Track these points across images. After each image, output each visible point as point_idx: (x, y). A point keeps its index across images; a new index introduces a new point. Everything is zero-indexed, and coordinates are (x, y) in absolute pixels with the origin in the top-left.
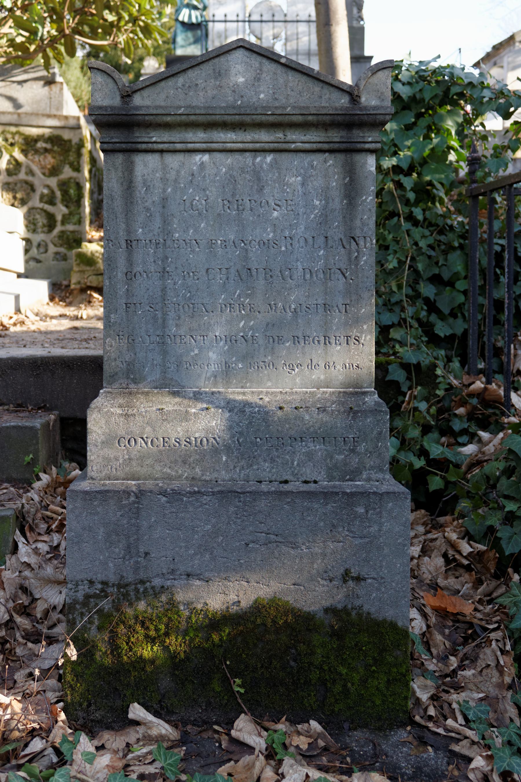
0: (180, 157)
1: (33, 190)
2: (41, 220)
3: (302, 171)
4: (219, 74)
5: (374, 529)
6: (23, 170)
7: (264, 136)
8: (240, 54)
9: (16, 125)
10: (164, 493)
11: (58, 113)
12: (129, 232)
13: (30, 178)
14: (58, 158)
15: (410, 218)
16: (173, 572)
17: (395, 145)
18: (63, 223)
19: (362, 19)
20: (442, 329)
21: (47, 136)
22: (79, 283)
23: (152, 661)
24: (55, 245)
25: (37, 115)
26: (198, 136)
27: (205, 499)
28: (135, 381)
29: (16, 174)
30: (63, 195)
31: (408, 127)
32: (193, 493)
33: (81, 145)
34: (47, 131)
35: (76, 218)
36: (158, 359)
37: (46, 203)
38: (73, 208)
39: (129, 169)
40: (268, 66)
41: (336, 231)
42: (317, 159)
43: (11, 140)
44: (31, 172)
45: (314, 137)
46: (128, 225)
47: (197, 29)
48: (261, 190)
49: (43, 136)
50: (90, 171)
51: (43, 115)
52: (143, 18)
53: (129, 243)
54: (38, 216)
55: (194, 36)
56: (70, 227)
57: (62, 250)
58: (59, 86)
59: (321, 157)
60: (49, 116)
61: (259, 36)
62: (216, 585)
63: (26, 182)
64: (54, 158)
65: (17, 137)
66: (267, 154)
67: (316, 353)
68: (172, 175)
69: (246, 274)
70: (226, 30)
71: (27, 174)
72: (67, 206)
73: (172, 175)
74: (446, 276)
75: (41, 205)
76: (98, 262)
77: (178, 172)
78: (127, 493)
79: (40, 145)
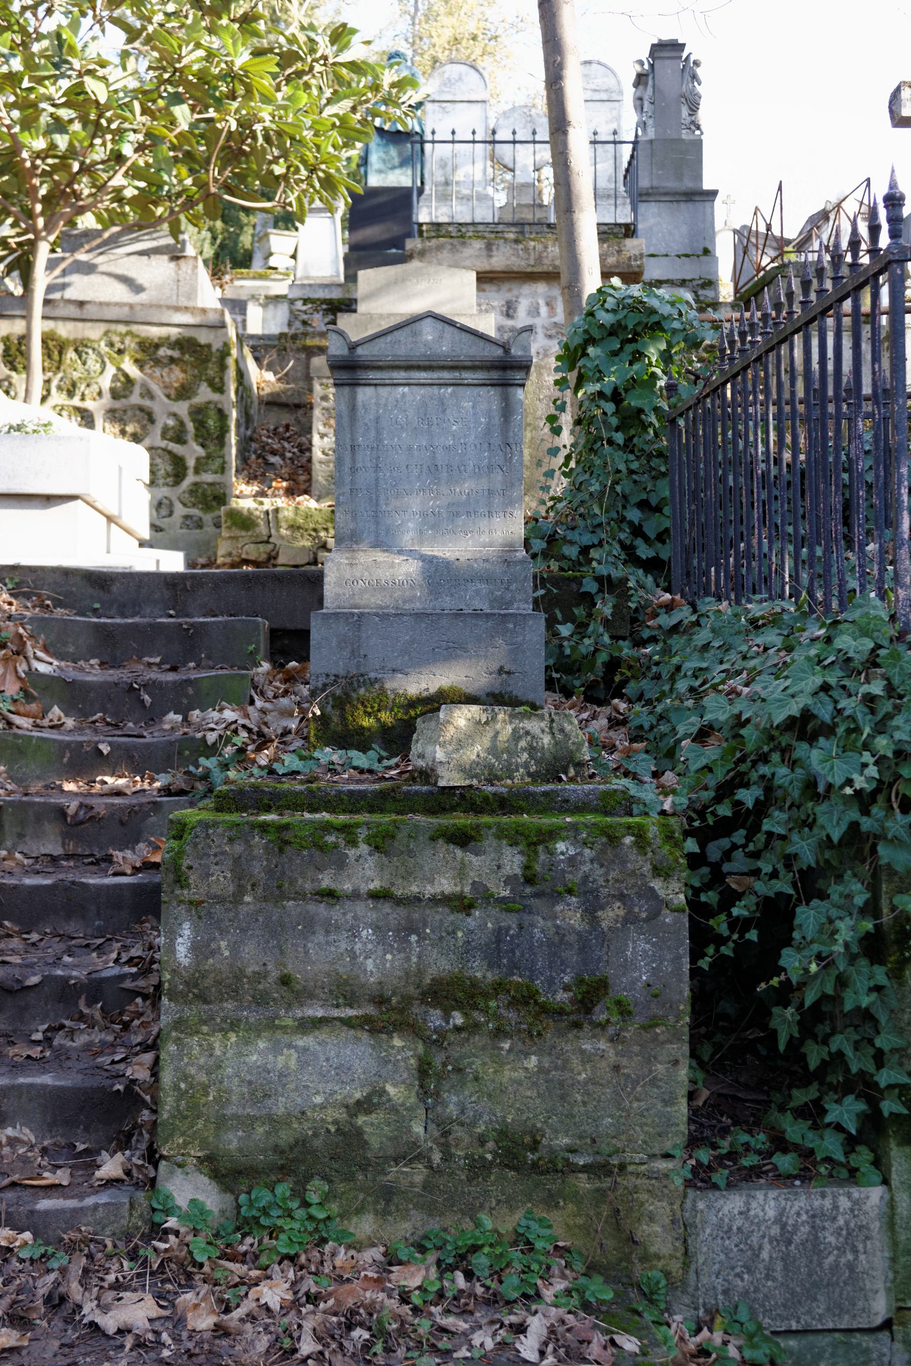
0: (388, 389)
1: (152, 421)
2: (165, 467)
4: (415, 334)
5: (520, 639)
6: (137, 390)
7: (446, 375)
8: (429, 320)
9: (127, 323)
10: (377, 615)
11: (190, 304)
12: (353, 440)
13: (147, 403)
14: (190, 372)
15: (610, 442)
16: (383, 668)
17: (600, 372)
18: (197, 471)
19: (698, 128)
20: (644, 551)
21: (173, 339)
22: (230, 554)
23: (369, 729)
24: (185, 505)
25: (159, 306)
26: (401, 375)
27: (405, 618)
28: (356, 543)
29: (125, 397)
30: (197, 429)
31: (615, 354)
32: (397, 615)
33: (225, 353)
34: (174, 332)
35: (218, 462)
36: (373, 527)
37: (171, 440)
38: (212, 448)
39: (353, 398)
40: (448, 329)
41: (497, 440)
42: (483, 391)
43: (118, 345)
44: (148, 394)
45: (480, 375)
46: (352, 434)
47: (406, 141)
48: (444, 411)
49: (168, 338)
50: (237, 392)
51: (169, 307)
52: (323, 167)
53: (353, 447)
55: (400, 154)
56: (208, 477)
57: (195, 512)
58: (191, 262)
59: (485, 389)
60: (177, 309)
61: (511, 166)
62: (412, 678)
63: (141, 409)
64: (185, 371)
65: (128, 340)
67: (483, 523)
68: (383, 401)
69: (434, 469)
70: (454, 156)
71: (142, 396)
72: (203, 446)
73: (383, 401)
74: (654, 502)
75: (164, 444)
76: (257, 525)
78: (353, 614)
79: (163, 352)
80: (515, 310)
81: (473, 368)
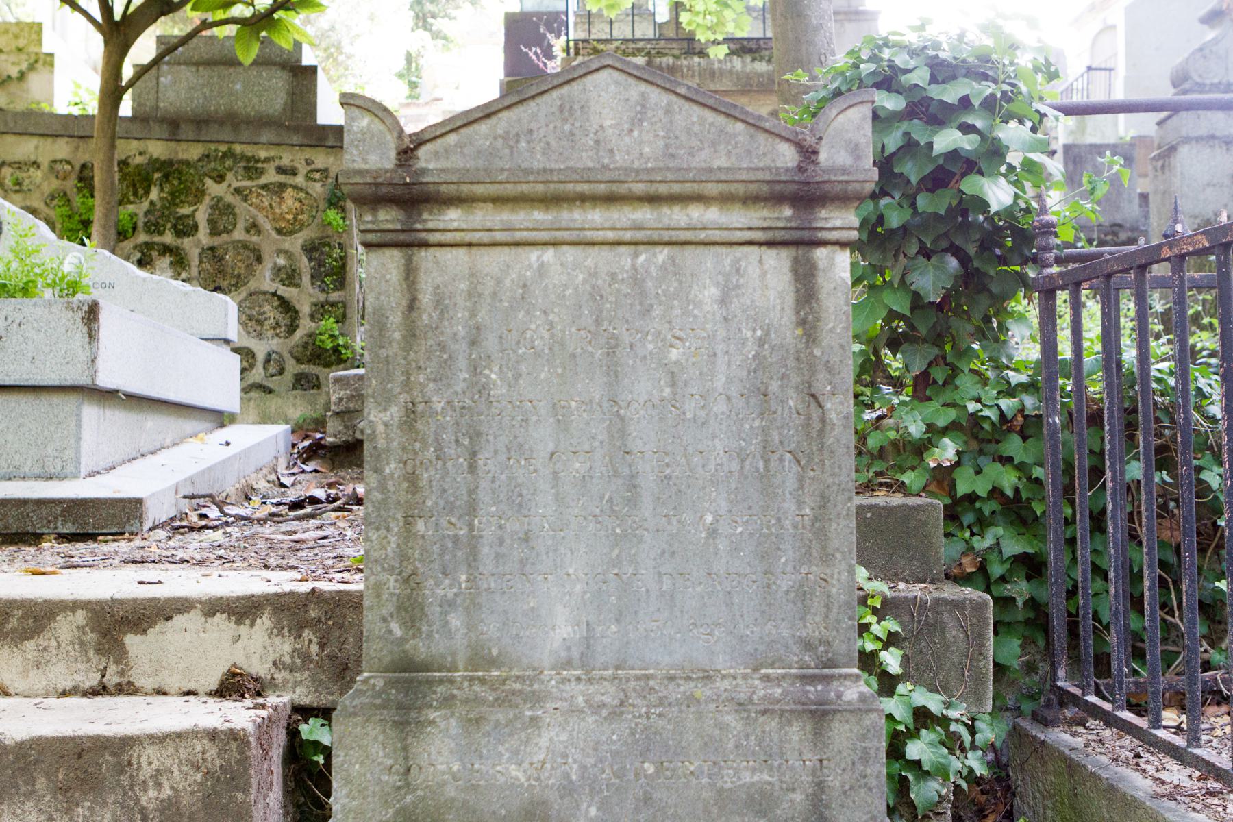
3: (720, 278)
24: (299, 361)
39: (410, 273)
45: (740, 218)
54: (267, 308)
63: (245, 246)
66: (658, 249)
77: (499, 282)
81: (726, 200)
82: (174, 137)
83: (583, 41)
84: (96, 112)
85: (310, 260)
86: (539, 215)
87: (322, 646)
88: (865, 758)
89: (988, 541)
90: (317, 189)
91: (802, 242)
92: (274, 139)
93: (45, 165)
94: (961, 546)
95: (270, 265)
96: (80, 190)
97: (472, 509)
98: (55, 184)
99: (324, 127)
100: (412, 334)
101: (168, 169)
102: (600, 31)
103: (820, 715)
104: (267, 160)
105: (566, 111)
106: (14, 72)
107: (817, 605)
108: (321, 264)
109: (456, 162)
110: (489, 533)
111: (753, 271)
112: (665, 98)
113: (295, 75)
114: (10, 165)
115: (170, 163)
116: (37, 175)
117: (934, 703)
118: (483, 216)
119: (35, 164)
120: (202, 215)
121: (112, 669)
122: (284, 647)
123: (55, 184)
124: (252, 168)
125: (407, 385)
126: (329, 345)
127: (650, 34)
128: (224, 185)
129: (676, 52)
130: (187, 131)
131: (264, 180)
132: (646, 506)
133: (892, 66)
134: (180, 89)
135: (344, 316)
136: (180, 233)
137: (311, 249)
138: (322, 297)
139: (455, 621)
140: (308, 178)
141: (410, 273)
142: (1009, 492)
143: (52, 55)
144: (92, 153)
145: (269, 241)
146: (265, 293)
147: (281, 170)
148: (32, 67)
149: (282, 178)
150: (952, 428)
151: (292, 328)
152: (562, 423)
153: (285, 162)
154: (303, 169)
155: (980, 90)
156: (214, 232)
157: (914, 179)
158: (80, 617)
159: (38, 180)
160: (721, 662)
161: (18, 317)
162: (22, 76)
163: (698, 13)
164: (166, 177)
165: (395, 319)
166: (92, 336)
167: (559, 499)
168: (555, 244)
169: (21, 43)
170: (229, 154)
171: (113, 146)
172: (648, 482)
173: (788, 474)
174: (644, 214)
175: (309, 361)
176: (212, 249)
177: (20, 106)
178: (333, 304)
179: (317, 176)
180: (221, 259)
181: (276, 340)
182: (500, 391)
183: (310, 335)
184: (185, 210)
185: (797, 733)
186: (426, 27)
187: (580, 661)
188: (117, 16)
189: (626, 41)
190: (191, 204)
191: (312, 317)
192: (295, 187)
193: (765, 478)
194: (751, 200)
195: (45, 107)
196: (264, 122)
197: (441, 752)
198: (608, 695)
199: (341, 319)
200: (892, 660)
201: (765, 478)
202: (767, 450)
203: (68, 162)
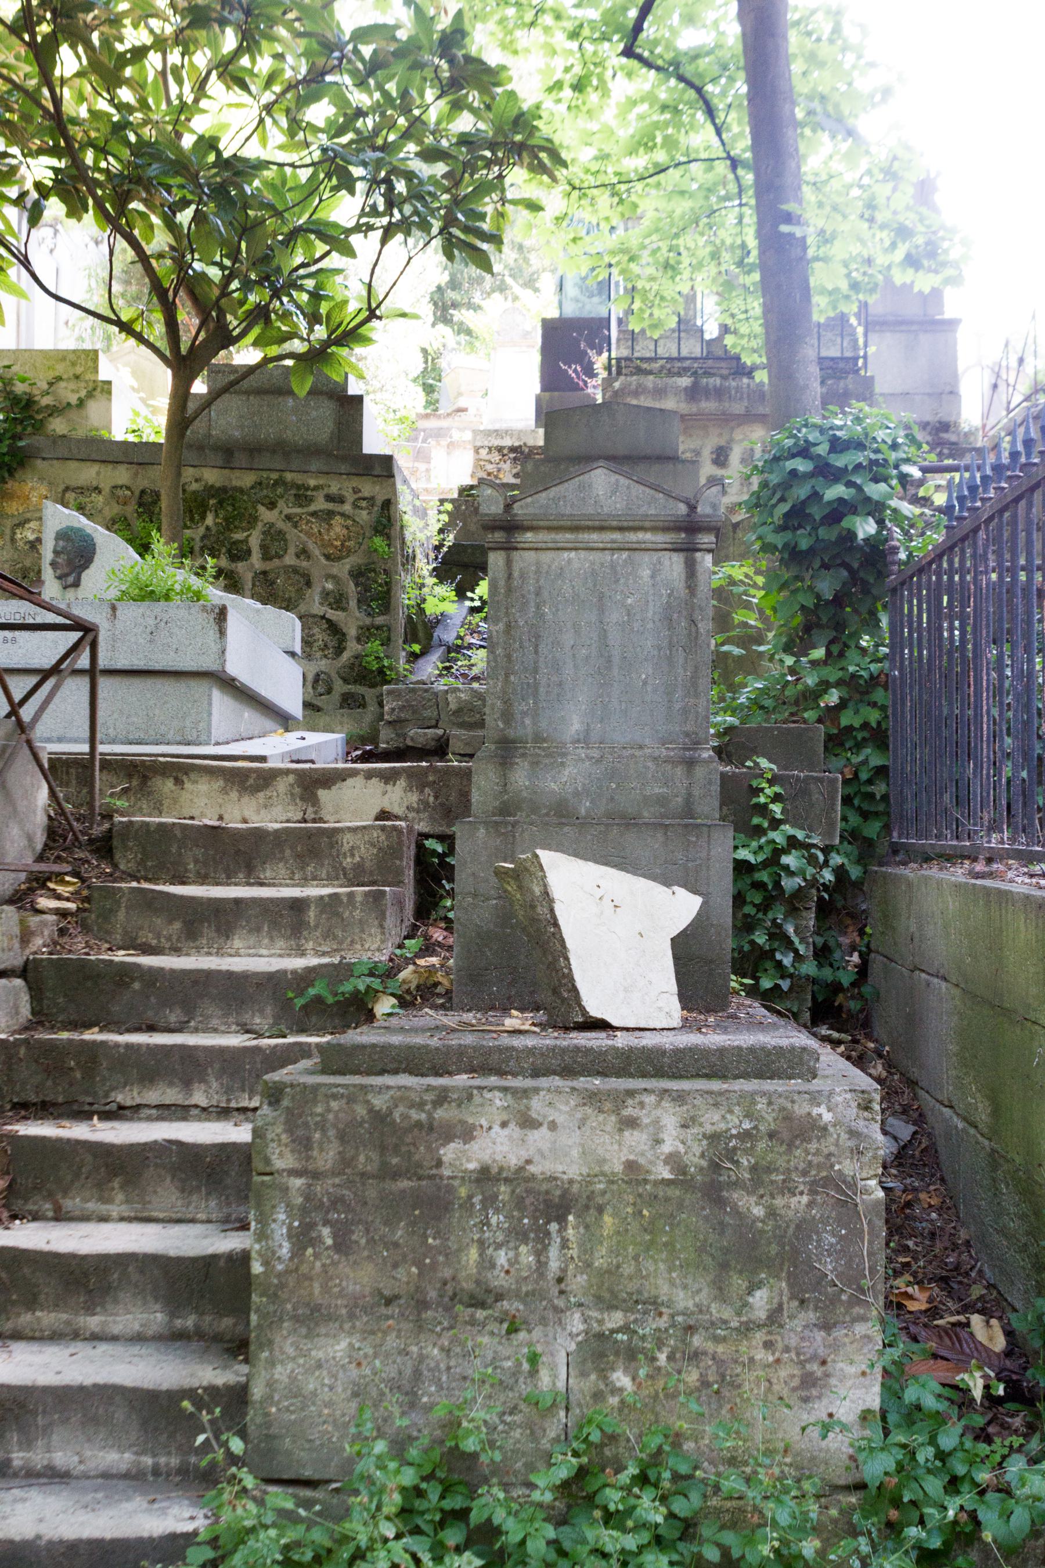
2: (320, 636)
24: (346, 681)
39: (509, 563)
45: (660, 538)
63: (295, 570)
80: (727, 457)
81: (654, 529)
82: (228, 464)
83: (627, 359)
84: (161, 439)
85: (357, 585)
86: (568, 536)
87: (436, 797)
88: (710, 783)
89: (861, 758)
90: (364, 516)
91: (689, 550)
92: (325, 469)
93: (106, 490)
94: (843, 762)
95: (319, 590)
96: (140, 515)
97: (536, 671)
98: (116, 509)
99: (371, 457)
100: (509, 590)
101: (223, 496)
102: (643, 350)
103: (690, 764)
104: (316, 488)
105: (581, 487)
106: (73, 399)
107: (691, 717)
108: (367, 589)
109: (531, 510)
110: (544, 681)
111: (667, 563)
112: (627, 482)
113: (342, 405)
114: (74, 490)
115: (224, 490)
116: (99, 500)
117: (800, 835)
118: (542, 536)
119: (97, 489)
120: (255, 541)
121: (310, 810)
122: (414, 798)
123: (116, 509)
124: (302, 496)
125: (507, 614)
126: (375, 666)
127: (697, 352)
128: (276, 512)
129: (725, 372)
130: (240, 459)
131: (313, 508)
132: (615, 671)
133: (806, 441)
134: (228, 420)
135: (389, 639)
136: (234, 558)
137: (358, 575)
138: (368, 621)
139: (527, 721)
140: (355, 506)
141: (509, 563)
142: (874, 725)
143: (109, 383)
144: (157, 478)
145: (318, 565)
146: (314, 616)
147: (329, 498)
148: (90, 395)
149: (330, 506)
150: (839, 684)
151: (339, 650)
152: (577, 632)
153: (334, 489)
154: (350, 497)
155: (860, 457)
156: (266, 557)
157: (817, 518)
158: (291, 778)
159: (100, 505)
160: (647, 741)
161: (165, 617)
162: (81, 403)
163: (742, 336)
164: (221, 503)
165: (502, 583)
166: (222, 633)
167: (575, 666)
168: (576, 549)
169: (79, 370)
170: (280, 482)
171: (179, 474)
172: (616, 660)
173: (680, 657)
174: (617, 536)
175: (355, 682)
176: (264, 573)
177: (81, 433)
178: (378, 628)
179: (364, 504)
180: (273, 583)
181: (324, 662)
182: (549, 617)
183: (356, 657)
184: (239, 536)
185: (679, 771)
186: (446, 320)
187: (584, 739)
188: (184, 349)
189: (670, 359)
190: (244, 530)
191: (358, 640)
192: (343, 515)
193: (670, 659)
194: (666, 529)
195: (104, 434)
196: (311, 451)
197: (520, 777)
198: (596, 754)
199: (386, 642)
200: (777, 808)
201: (670, 659)
202: (671, 646)
203: (128, 488)
